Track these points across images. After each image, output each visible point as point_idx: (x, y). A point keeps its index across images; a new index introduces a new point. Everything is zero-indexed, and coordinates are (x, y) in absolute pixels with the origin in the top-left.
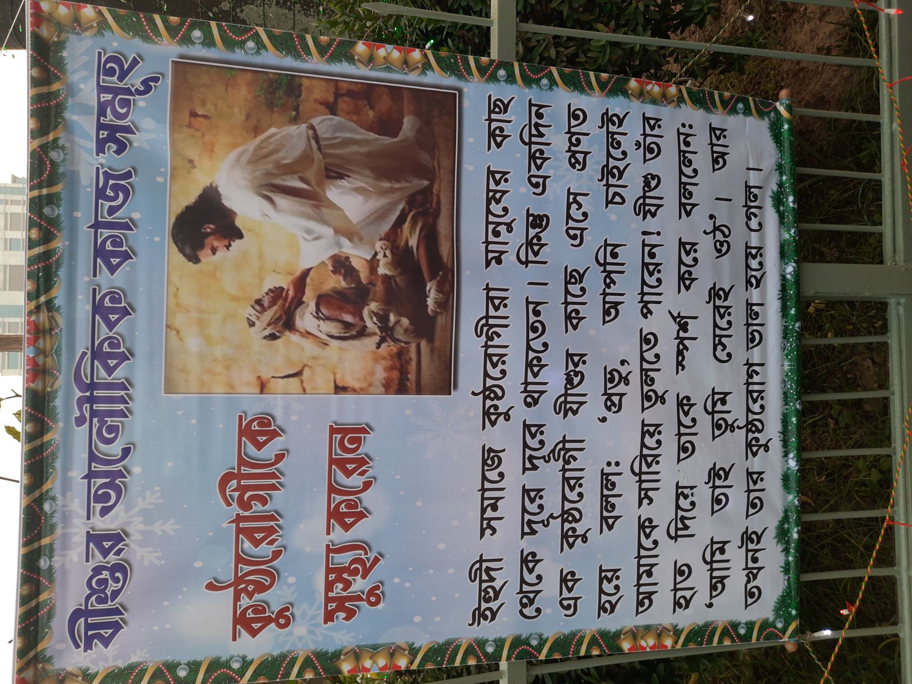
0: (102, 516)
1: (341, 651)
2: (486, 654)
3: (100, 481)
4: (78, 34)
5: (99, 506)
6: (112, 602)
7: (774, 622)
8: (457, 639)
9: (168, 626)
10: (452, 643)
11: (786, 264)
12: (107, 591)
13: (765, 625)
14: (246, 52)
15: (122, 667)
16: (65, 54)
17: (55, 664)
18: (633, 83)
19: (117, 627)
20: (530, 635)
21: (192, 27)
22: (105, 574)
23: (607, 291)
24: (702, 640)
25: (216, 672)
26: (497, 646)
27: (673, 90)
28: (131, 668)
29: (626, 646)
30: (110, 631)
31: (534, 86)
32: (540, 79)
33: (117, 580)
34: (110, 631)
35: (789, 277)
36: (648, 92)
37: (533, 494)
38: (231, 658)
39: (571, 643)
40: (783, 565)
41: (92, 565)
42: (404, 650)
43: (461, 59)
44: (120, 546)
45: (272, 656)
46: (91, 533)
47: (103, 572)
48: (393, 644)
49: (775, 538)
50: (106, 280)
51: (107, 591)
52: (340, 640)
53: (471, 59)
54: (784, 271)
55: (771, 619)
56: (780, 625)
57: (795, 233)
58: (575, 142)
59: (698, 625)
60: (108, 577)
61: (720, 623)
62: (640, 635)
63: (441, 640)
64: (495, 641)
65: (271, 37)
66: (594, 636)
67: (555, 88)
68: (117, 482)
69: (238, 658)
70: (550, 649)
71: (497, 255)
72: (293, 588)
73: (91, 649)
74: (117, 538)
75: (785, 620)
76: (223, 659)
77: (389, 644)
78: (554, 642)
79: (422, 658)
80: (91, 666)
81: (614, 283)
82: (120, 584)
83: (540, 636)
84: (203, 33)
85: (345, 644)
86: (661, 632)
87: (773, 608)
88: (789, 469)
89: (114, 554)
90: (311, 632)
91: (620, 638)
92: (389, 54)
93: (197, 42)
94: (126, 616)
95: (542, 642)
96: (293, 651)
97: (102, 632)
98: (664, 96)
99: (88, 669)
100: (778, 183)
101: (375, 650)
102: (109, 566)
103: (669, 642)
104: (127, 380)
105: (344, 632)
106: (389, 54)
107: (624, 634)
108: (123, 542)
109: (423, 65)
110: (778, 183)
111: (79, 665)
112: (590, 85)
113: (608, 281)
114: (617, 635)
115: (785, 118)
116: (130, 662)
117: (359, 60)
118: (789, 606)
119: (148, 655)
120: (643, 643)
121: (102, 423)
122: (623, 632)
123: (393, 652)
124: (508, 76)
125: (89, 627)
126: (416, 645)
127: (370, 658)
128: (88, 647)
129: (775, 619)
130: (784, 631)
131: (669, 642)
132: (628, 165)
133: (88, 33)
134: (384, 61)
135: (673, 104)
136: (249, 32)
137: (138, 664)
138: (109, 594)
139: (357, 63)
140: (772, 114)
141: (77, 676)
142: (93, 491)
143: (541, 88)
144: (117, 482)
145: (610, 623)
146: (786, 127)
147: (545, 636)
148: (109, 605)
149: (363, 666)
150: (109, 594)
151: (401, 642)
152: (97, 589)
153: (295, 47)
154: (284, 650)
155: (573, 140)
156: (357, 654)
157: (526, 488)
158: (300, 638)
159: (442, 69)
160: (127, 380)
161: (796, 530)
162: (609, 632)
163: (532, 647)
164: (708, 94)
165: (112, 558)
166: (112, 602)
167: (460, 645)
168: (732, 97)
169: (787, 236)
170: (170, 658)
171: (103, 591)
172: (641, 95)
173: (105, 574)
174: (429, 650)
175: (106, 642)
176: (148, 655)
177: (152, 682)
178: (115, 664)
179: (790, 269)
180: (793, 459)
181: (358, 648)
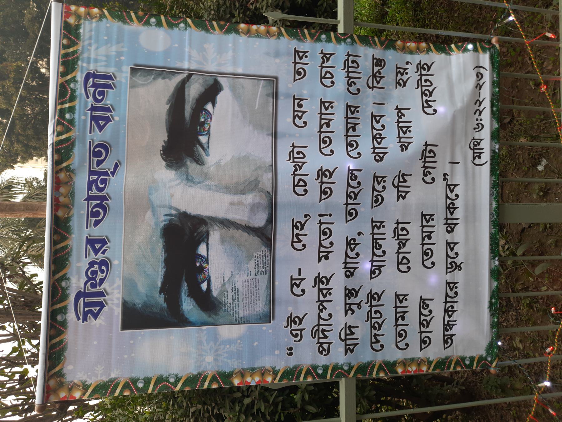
0: (95, 227)
1: (233, 371)
2: (138, 389)
3: (95, 203)
6: (99, 287)
8: (300, 365)
10: (298, 367)
12: (96, 279)
13: (481, 358)
14: (179, 29)
15: (106, 381)
17: (67, 378)
21: (321, 34)
22: (96, 267)
23: (400, 120)
24: (444, 367)
25: (161, 384)
28: (111, 381)
29: (400, 370)
30: (98, 308)
31: (343, 43)
32: (179, 24)
33: (102, 272)
34: (98, 308)
37: (380, 179)
38: (169, 375)
39: (367, 368)
41: (89, 260)
44: (104, 248)
46: (89, 238)
47: (95, 265)
48: (263, 367)
50: (98, 136)
51: (96, 279)
52: (232, 364)
53: (306, 31)
55: (484, 355)
56: (489, 359)
59: (441, 358)
60: (98, 269)
62: (408, 364)
66: (381, 364)
67: (354, 44)
68: (103, 203)
69: (173, 376)
70: (355, 372)
71: (327, 121)
72: (205, 332)
73: (87, 321)
74: (103, 242)
76: (165, 376)
77: (261, 367)
78: (357, 368)
79: (281, 377)
80: (88, 380)
81: (404, 116)
82: (104, 274)
83: (350, 364)
84: (156, 20)
85: (236, 367)
87: (485, 349)
89: (101, 253)
91: (396, 366)
93: (153, 24)
94: (107, 298)
96: (205, 372)
97: (93, 308)
99: (86, 382)
100: (492, 324)
102: (98, 261)
103: (424, 369)
104: (113, 74)
105: (235, 359)
107: (399, 363)
108: (107, 245)
109: (278, 33)
111: (81, 379)
112: (213, 27)
113: (400, 114)
116: (110, 378)
117: (242, 32)
120: (410, 369)
123: (263, 373)
124: (327, 38)
125: (86, 305)
126: (277, 369)
127: (250, 376)
128: (85, 319)
129: (487, 355)
131: (424, 369)
137: (115, 379)
138: (98, 281)
142: (90, 209)
143: (347, 44)
144: (103, 203)
147: (352, 365)
149: (246, 381)
150: (98, 281)
151: (268, 365)
152: (91, 279)
153: (206, 26)
154: (200, 371)
156: (242, 374)
157: (376, 175)
158: (209, 363)
159: (289, 35)
160: (113, 74)
163: (170, 383)
165: (100, 256)
166: (99, 287)
171: (94, 279)
173: (96, 267)
174: (284, 372)
175: (96, 316)
176: (120, 374)
177: (123, 390)
178: (101, 379)
181: (243, 370)
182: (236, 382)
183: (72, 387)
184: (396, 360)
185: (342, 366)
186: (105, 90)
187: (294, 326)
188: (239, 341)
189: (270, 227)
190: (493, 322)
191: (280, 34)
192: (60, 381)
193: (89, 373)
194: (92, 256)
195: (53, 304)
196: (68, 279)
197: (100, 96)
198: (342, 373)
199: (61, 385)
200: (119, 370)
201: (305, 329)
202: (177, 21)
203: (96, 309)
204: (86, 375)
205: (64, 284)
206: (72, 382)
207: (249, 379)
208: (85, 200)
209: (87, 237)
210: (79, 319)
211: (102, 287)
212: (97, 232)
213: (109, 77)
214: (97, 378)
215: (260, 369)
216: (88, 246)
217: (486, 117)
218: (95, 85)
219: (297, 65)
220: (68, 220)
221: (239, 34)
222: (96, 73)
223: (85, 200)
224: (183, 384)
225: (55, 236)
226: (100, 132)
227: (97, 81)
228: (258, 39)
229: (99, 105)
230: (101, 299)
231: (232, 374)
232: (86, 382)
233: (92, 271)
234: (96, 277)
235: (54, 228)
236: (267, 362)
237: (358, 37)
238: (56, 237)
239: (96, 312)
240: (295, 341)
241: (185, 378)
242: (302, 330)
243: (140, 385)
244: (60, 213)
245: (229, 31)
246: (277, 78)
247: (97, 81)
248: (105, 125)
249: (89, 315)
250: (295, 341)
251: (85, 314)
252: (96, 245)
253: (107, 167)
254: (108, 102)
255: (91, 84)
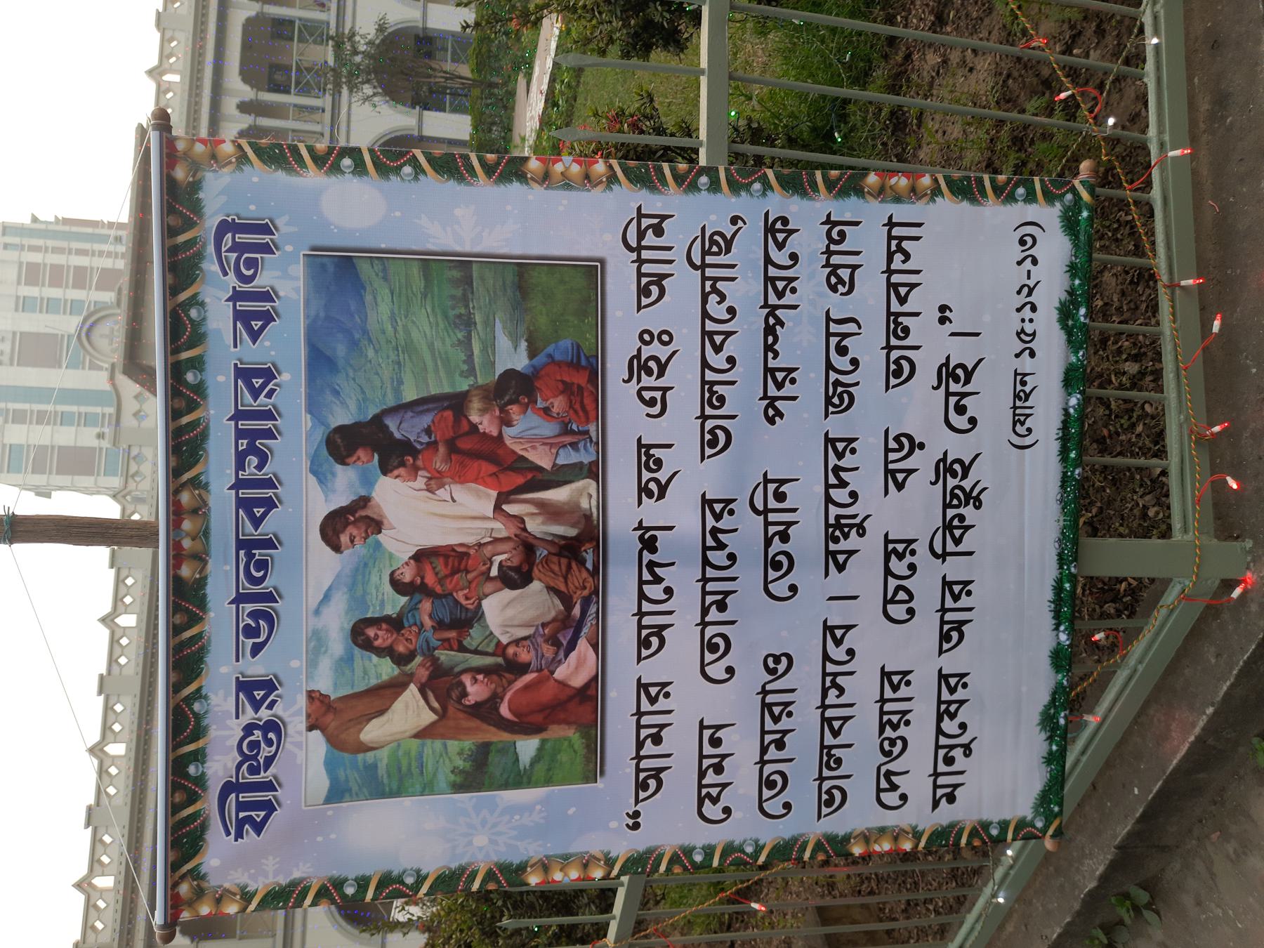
0: (253, 657)
1: (527, 862)
4: (215, 171)
5: (250, 642)
7: (1032, 821)
9: (333, 836)
11: (1070, 394)
14: (402, 179)
16: (201, 195)
18: (872, 179)
19: (269, 807)
20: (745, 841)
22: (258, 735)
26: (706, 854)
27: (926, 181)
28: (294, 884)
30: (262, 814)
31: (743, 193)
32: (401, 166)
34: (262, 814)
35: (1072, 411)
36: (891, 187)
38: (404, 872)
40: (1046, 755)
42: (599, 860)
43: (654, 168)
44: (271, 698)
45: (449, 869)
49: (1039, 724)
54: (1067, 404)
56: (1039, 824)
57: (1083, 356)
58: (837, 238)
59: (941, 826)
60: (260, 738)
61: (968, 823)
62: (873, 839)
63: (641, 848)
64: (703, 848)
65: (430, 159)
66: (819, 840)
74: (269, 686)
75: (1046, 818)
80: (250, 882)
83: (756, 841)
84: (354, 160)
85: (531, 854)
86: (898, 834)
87: (1032, 805)
88: (1059, 644)
90: (492, 841)
92: (567, 169)
95: (759, 849)
97: (253, 814)
98: (913, 190)
99: (246, 886)
100: (1069, 289)
101: (566, 860)
102: (261, 723)
106: (567, 169)
107: (855, 838)
110: (1069, 289)
111: (237, 881)
114: (847, 839)
115: (1086, 203)
116: (292, 877)
117: (532, 179)
118: (1050, 802)
119: (311, 870)
121: (250, 556)
122: (530, 863)
125: (241, 806)
127: (561, 870)
128: (239, 835)
129: (1034, 817)
130: (1044, 830)
132: (675, 352)
133: (225, 170)
134: (561, 178)
135: (925, 200)
136: (405, 155)
137: (301, 880)
138: (262, 761)
139: (530, 182)
140: (1069, 197)
141: (235, 894)
143: (751, 195)
145: (837, 824)
146: (1085, 214)
148: (262, 777)
150: (262, 761)
152: (250, 757)
153: (457, 169)
154: (463, 862)
155: (835, 235)
156: (545, 867)
158: (481, 849)
161: (1062, 714)
162: (837, 836)
164: (975, 180)
165: (264, 714)
166: (265, 772)
167: (663, 854)
168: (1009, 180)
169: (1074, 359)
170: (335, 873)
171: (255, 757)
172: (881, 193)
173: (258, 735)
176: (311, 870)
179: (1073, 401)
180: (1063, 632)
182: (534, 880)
183: (221, 896)
184: (849, 831)
185: (741, 845)
186: (258, 256)
187: (647, 381)
188: (538, 807)
189: (594, 732)
190: (1050, 753)
191: (612, 179)
192: (198, 885)
193: (253, 871)
194: (249, 715)
195: (175, 748)
196: (206, 698)
197: (248, 269)
198: (742, 859)
199: (199, 893)
200: (309, 865)
201: (672, 388)
202: (397, 161)
203: (259, 815)
204: (246, 874)
205: (197, 707)
206: (220, 887)
207: (558, 876)
208: (230, 488)
209: (236, 365)
210: (228, 834)
211: (272, 770)
212: (256, 668)
213: (265, 229)
214: (267, 877)
215: (580, 856)
216: (240, 382)
217: (1047, 325)
218: (237, 247)
219: (642, 731)
220: (201, 583)
221: (527, 184)
222: (237, 221)
223: (230, 488)
224: (431, 887)
225: (178, 616)
226: (259, 836)
227: (242, 238)
228: (567, 193)
229: (246, 288)
230: (268, 795)
231: (526, 867)
232: (246, 886)
233: (251, 741)
234: (258, 753)
235: (172, 384)
236: (593, 844)
237: (777, 178)
238: (172, 221)
239: (258, 820)
240: (648, 415)
241: (435, 876)
242: (665, 390)
243: (350, 891)
244: (186, 571)
245: (505, 178)
246: (602, 262)
247: (242, 238)
248: (262, 328)
249: (247, 826)
250: (648, 415)
251: (240, 824)
252: (255, 693)
253: (271, 531)
254: (263, 281)
255: (230, 244)
